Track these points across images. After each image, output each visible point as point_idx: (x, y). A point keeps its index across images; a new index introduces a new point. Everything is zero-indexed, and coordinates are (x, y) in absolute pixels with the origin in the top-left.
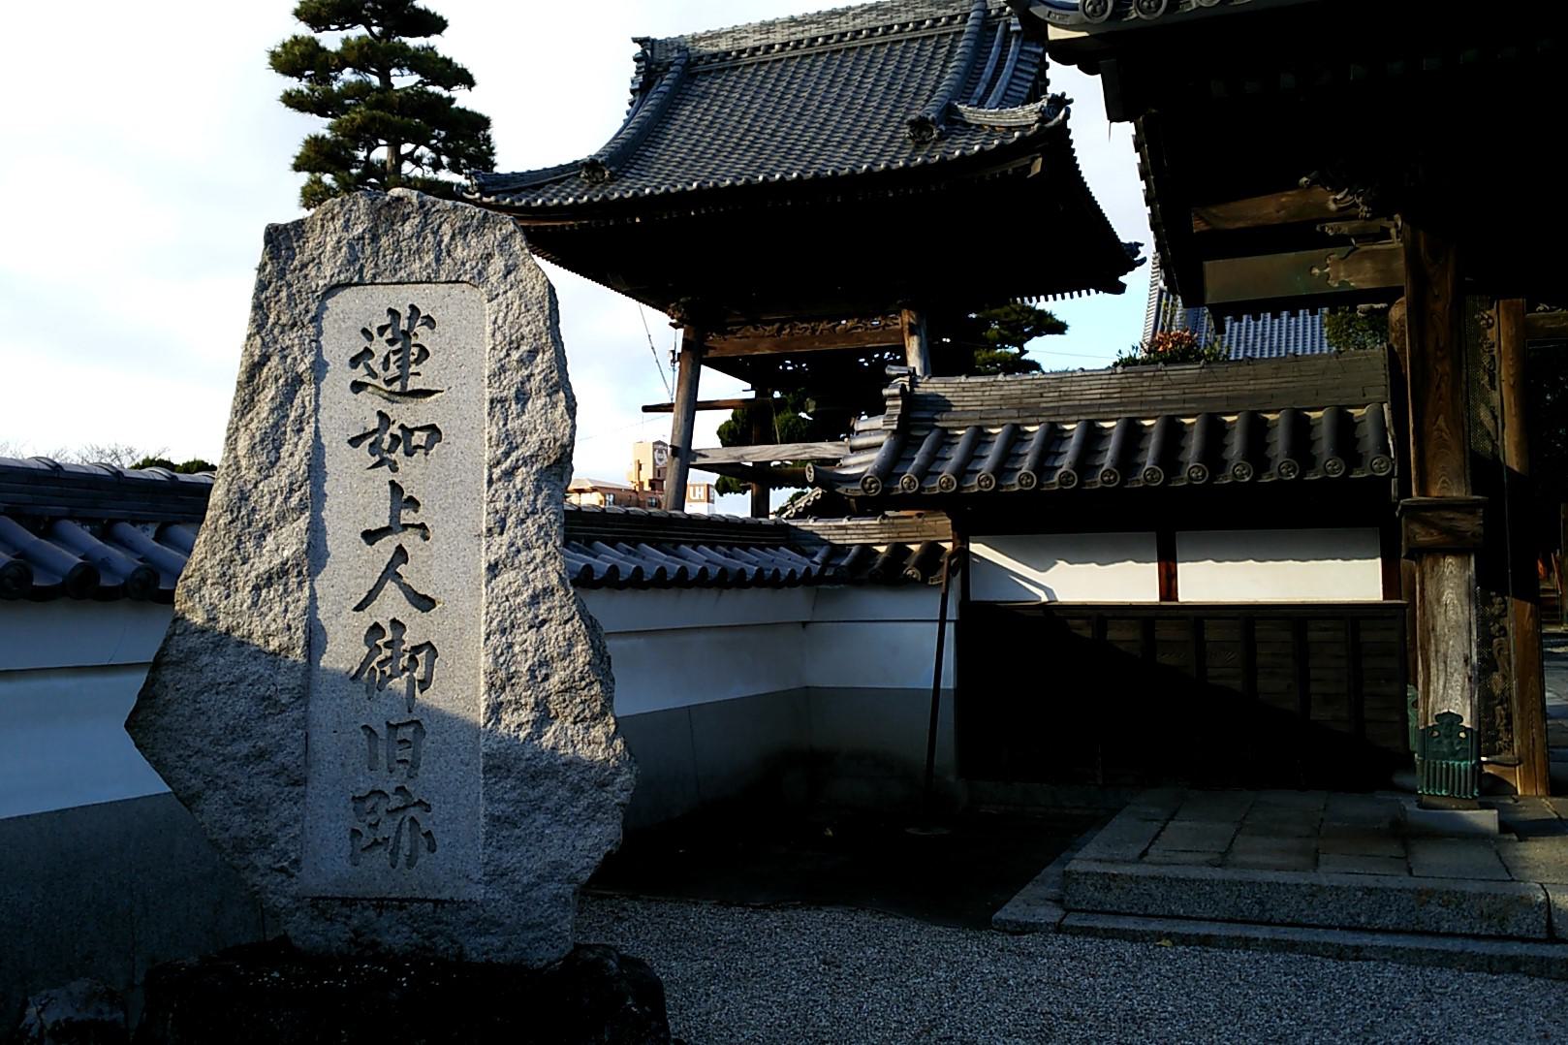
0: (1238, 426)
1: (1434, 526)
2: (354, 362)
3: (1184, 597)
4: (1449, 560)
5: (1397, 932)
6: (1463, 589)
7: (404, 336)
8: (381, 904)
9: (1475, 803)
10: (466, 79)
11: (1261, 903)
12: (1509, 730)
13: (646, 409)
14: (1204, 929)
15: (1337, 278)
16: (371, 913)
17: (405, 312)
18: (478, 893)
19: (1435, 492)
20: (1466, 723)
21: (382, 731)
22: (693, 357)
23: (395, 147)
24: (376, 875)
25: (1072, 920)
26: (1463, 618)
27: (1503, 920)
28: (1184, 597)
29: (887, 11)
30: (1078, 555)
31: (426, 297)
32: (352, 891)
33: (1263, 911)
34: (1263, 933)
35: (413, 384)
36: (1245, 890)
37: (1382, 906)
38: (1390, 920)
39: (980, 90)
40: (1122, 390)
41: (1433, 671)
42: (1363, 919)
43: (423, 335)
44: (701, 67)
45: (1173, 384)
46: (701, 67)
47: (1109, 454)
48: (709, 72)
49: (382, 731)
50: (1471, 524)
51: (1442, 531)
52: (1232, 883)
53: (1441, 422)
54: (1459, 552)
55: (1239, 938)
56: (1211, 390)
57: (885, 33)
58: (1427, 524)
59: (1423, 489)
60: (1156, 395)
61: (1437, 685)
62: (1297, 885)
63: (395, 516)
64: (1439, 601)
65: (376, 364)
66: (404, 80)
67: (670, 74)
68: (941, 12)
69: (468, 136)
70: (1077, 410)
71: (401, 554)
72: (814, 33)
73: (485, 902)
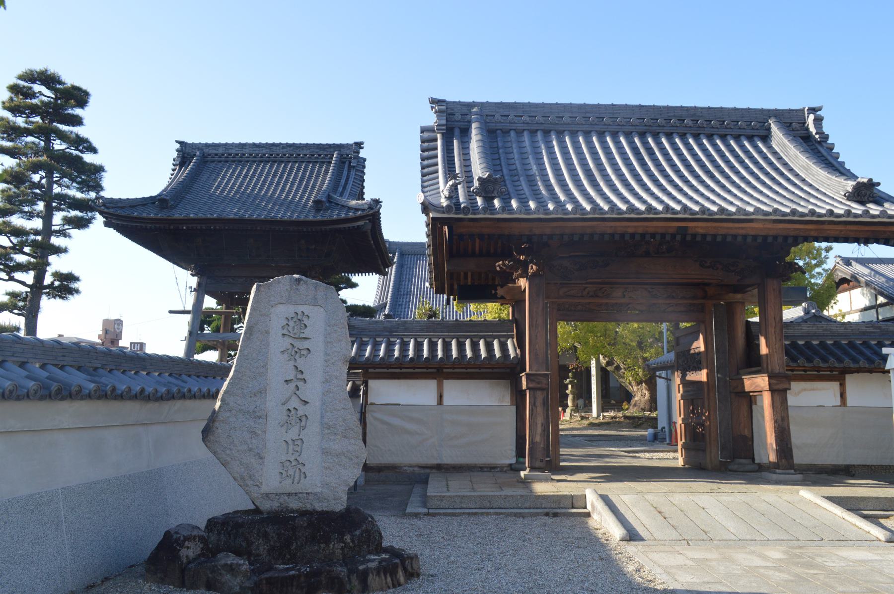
2: (283, 328)
7: (300, 321)
8: (289, 494)
10: (94, 150)
13: (171, 312)
14: (474, 511)
16: (286, 498)
17: (300, 313)
18: (319, 490)
21: (290, 442)
22: (201, 291)
23: (49, 176)
24: (287, 486)
25: (431, 511)
31: (306, 309)
32: (279, 491)
34: (492, 511)
35: (302, 336)
38: (527, 505)
39: (340, 189)
43: (306, 321)
44: (209, 158)
46: (209, 158)
48: (213, 162)
49: (290, 442)
63: (296, 376)
65: (290, 329)
66: (58, 145)
67: (197, 160)
69: (90, 176)
71: (297, 388)
72: (264, 152)
73: (321, 493)
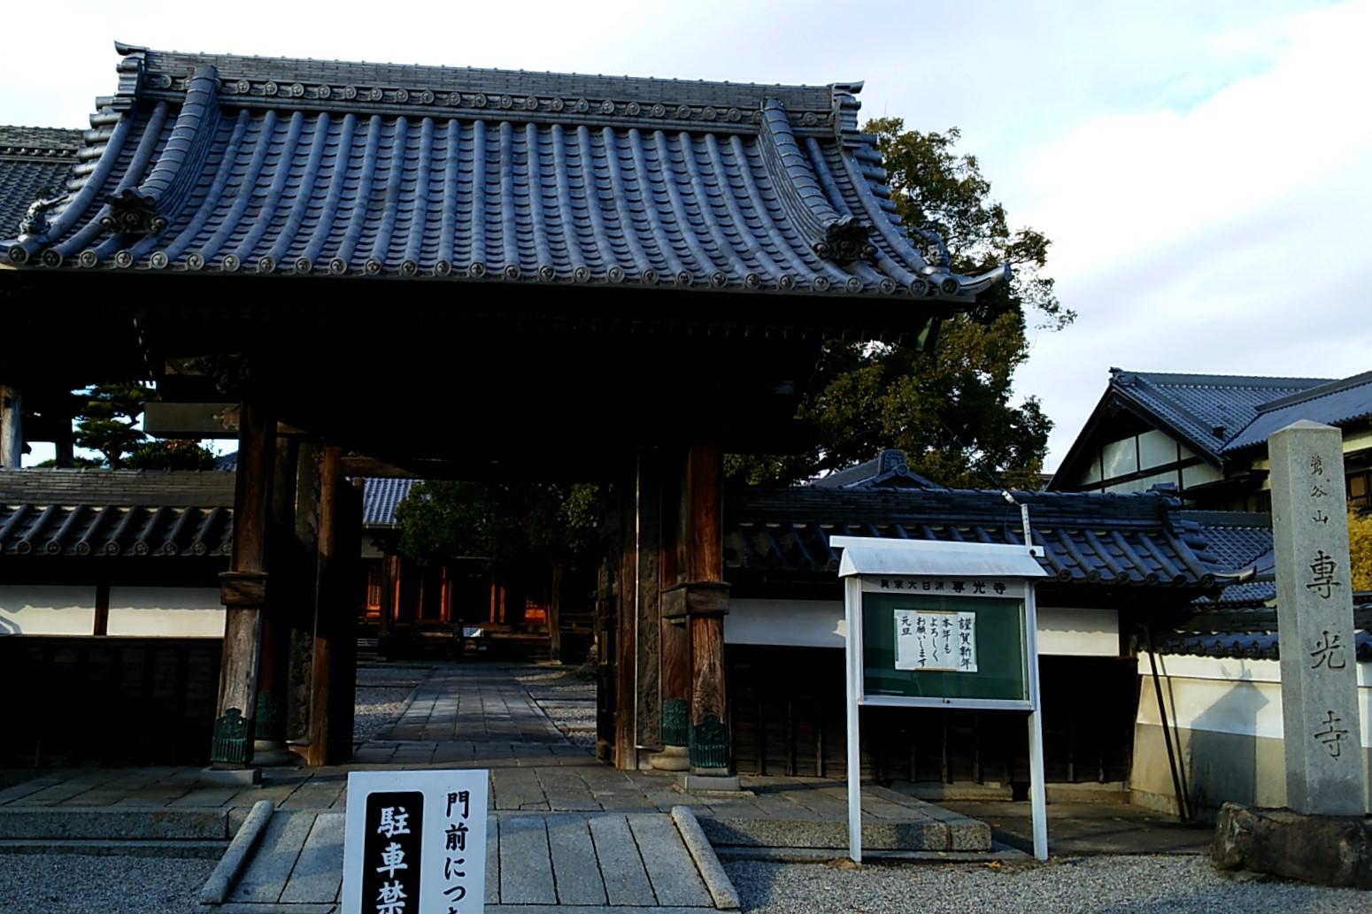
0: (154, 517)
1: (237, 589)
3: (111, 632)
4: (245, 612)
5: (142, 839)
6: (250, 631)
9: (243, 766)
11: (63, 826)
12: (307, 722)
15: (227, 423)
19: (241, 568)
20: (243, 715)
26: (248, 648)
27: (201, 830)
28: (111, 632)
29: (17, 135)
30: (41, 600)
33: (64, 831)
36: (55, 819)
37: (135, 824)
38: (138, 833)
40: (84, 484)
41: (228, 682)
42: (123, 833)
45: (117, 484)
47: (60, 531)
50: (258, 590)
51: (243, 594)
52: (47, 814)
53: (249, 525)
54: (251, 607)
55: (39, 847)
56: (145, 489)
57: (12, 153)
58: (233, 588)
59: (235, 569)
60: (106, 491)
61: (229, 691)
62: (87, 814)
64: (236, 637)
68: (63, 146)
70: (48, 497)
